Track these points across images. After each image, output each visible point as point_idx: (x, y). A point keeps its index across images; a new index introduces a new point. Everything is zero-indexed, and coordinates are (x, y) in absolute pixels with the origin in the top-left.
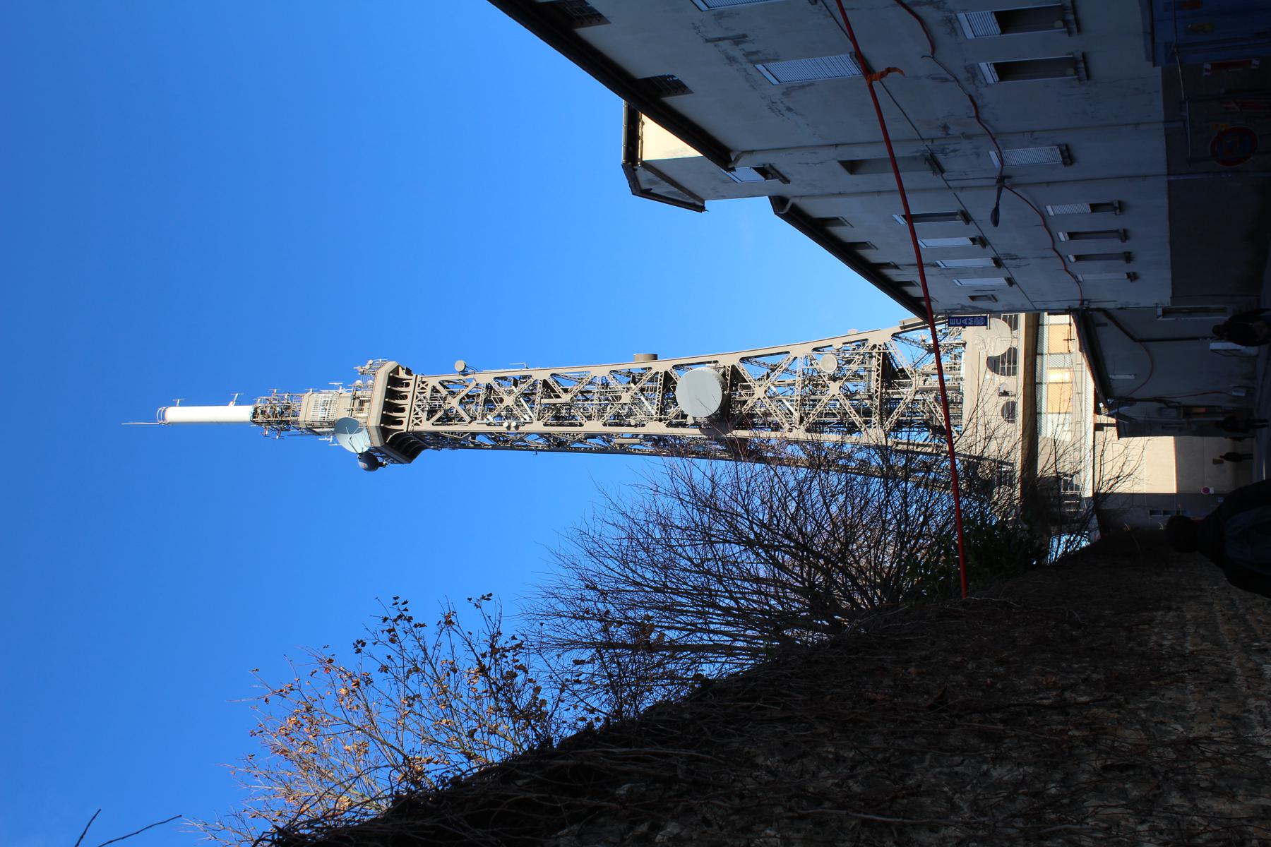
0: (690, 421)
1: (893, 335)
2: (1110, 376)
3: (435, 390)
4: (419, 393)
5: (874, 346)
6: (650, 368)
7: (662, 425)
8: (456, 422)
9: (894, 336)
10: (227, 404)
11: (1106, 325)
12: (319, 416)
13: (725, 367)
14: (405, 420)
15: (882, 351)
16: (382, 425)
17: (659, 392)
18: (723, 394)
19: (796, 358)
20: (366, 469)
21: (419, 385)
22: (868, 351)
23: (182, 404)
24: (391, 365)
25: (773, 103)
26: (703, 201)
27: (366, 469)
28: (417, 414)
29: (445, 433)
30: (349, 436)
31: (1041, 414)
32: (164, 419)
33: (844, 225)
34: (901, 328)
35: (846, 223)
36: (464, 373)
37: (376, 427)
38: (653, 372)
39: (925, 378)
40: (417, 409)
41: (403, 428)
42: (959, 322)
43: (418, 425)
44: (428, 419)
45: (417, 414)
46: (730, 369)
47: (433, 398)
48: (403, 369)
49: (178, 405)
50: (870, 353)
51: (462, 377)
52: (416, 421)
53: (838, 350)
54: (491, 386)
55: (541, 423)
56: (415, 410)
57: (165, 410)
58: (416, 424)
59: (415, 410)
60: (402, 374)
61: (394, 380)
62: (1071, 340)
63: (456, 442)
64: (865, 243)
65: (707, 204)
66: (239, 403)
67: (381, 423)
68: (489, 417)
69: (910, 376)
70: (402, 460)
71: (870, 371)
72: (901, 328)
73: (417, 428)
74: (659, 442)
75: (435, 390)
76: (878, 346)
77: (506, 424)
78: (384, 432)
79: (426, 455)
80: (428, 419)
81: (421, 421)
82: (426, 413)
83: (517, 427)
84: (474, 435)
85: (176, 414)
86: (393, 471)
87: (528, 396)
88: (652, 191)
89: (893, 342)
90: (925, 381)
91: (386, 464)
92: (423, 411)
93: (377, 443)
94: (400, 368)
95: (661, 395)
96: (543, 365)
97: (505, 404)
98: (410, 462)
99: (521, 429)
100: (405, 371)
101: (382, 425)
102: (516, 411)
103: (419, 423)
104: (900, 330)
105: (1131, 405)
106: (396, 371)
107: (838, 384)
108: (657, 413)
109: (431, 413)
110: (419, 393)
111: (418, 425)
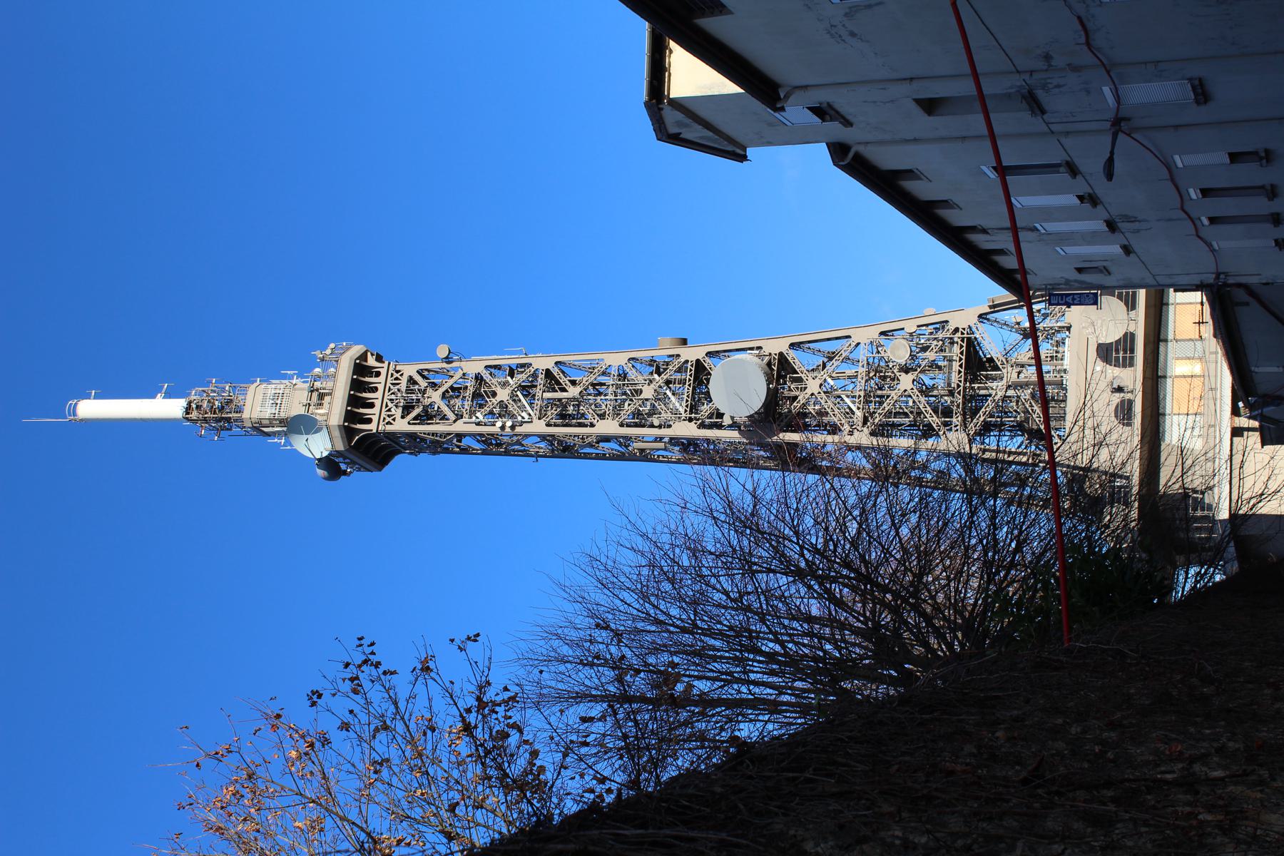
0: (727, 421)
1: (980, 316)
2: (1253, 368)
3: (411, 381)
4: (392, 384)
5: (956, 330)
6: (678, 356)
7: (693, 425)
8: (438, 421)
9: (982, 317)
10: (154, 397)
11: (1247, 304)
12: (268, 412)
13: (770, 354)
14: (375, 419)
15: (965, 336)
16: (346, 424)
17: (689, 385)
18: (768, 388)
19: (858, 344)
20: (326, 479)
21: (392, 375)
22: (948, 336)
23: (97, 397)
24: (357, 350)
25: (832, 26)
26: (744, 149)
27: (326, 479)
28: (389, 410)
29: (424, 434)
30: (305, 437)
31: (1164, 415)
32: (75, 414)
33: (920, 179)
34: (990, 307)
35: (923, 177)
36: (448, 360)
37: (339, 426)
38: (682, 359)
39: (1019, 369)
40: (390, 405)
41: (372, 427)
42: (1062, 300)
43: (391, 424)
44: (403, 417)
45: (389, 410)
46: (777, 357)
47: (409, 391)
48: (372, 355)
49: (92, 397)
50: (951, 338)
51: (445, 365)
52: (388, 419)
53: (911, 334)
54: (482, 377)
55: (542, 422)
56: (387, 406)
57: (76, 404)
58: (389, 423)
59: (387, 406)
60: (371, 361)
61: (361, 369)
62: (1203, 323)
63: (438, 446)
64: (1002, 250)
65: (750, 152)
66: (169, 395)
67: (345, 421)
68: (478, 414)
69: (1001, 366)
70: (368, 466)
71: (951, 361)
72: (990, 307)
73: (389, 428)
74: (688, 446)
75: (411, 381)
76: (961, 330)
77: (499, 424)
78: (348, 432)
79: (401, 462)
80: (403, 417)
81: (394, 420)
82: (400, 410)
83: (513, 427)
84: (460, 436)
85: (90, 408)
86: (359, 480)
87: (527, 389)
88: (681, 136)
89: (979, 325)
90: (1019, 373)
91: (351, 472)
92: (397, 406)
93: (340, 446)
94: (369, 354)
95: (691, 389)
96: (547, 352)
97: (498, 398)
98: (380, 470)
99: (518, 429)
100: (374, 357)
101: (346, 424)
102: (512, 408)
103: (392, 422)
104: (988, 310)
105: (1278, 405)
106: (364, 357)
107: (911, 376)
108: (686, 411)
109: (407, 409)
110: (392, 384)
111: (391, 424)
